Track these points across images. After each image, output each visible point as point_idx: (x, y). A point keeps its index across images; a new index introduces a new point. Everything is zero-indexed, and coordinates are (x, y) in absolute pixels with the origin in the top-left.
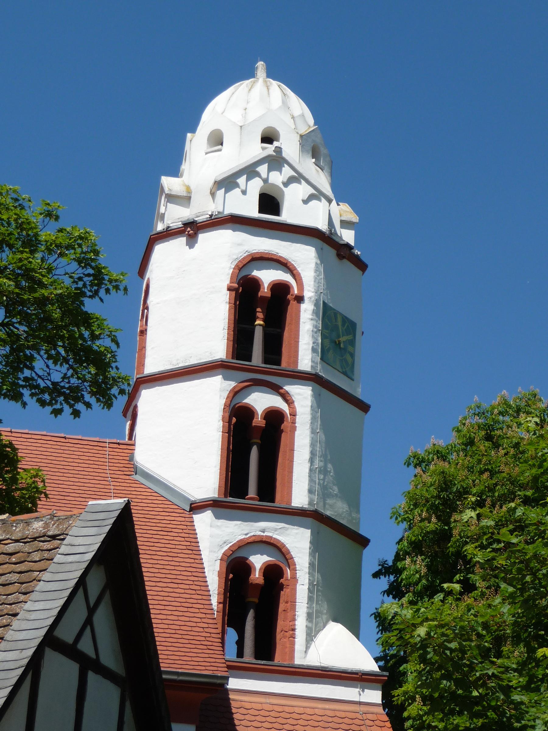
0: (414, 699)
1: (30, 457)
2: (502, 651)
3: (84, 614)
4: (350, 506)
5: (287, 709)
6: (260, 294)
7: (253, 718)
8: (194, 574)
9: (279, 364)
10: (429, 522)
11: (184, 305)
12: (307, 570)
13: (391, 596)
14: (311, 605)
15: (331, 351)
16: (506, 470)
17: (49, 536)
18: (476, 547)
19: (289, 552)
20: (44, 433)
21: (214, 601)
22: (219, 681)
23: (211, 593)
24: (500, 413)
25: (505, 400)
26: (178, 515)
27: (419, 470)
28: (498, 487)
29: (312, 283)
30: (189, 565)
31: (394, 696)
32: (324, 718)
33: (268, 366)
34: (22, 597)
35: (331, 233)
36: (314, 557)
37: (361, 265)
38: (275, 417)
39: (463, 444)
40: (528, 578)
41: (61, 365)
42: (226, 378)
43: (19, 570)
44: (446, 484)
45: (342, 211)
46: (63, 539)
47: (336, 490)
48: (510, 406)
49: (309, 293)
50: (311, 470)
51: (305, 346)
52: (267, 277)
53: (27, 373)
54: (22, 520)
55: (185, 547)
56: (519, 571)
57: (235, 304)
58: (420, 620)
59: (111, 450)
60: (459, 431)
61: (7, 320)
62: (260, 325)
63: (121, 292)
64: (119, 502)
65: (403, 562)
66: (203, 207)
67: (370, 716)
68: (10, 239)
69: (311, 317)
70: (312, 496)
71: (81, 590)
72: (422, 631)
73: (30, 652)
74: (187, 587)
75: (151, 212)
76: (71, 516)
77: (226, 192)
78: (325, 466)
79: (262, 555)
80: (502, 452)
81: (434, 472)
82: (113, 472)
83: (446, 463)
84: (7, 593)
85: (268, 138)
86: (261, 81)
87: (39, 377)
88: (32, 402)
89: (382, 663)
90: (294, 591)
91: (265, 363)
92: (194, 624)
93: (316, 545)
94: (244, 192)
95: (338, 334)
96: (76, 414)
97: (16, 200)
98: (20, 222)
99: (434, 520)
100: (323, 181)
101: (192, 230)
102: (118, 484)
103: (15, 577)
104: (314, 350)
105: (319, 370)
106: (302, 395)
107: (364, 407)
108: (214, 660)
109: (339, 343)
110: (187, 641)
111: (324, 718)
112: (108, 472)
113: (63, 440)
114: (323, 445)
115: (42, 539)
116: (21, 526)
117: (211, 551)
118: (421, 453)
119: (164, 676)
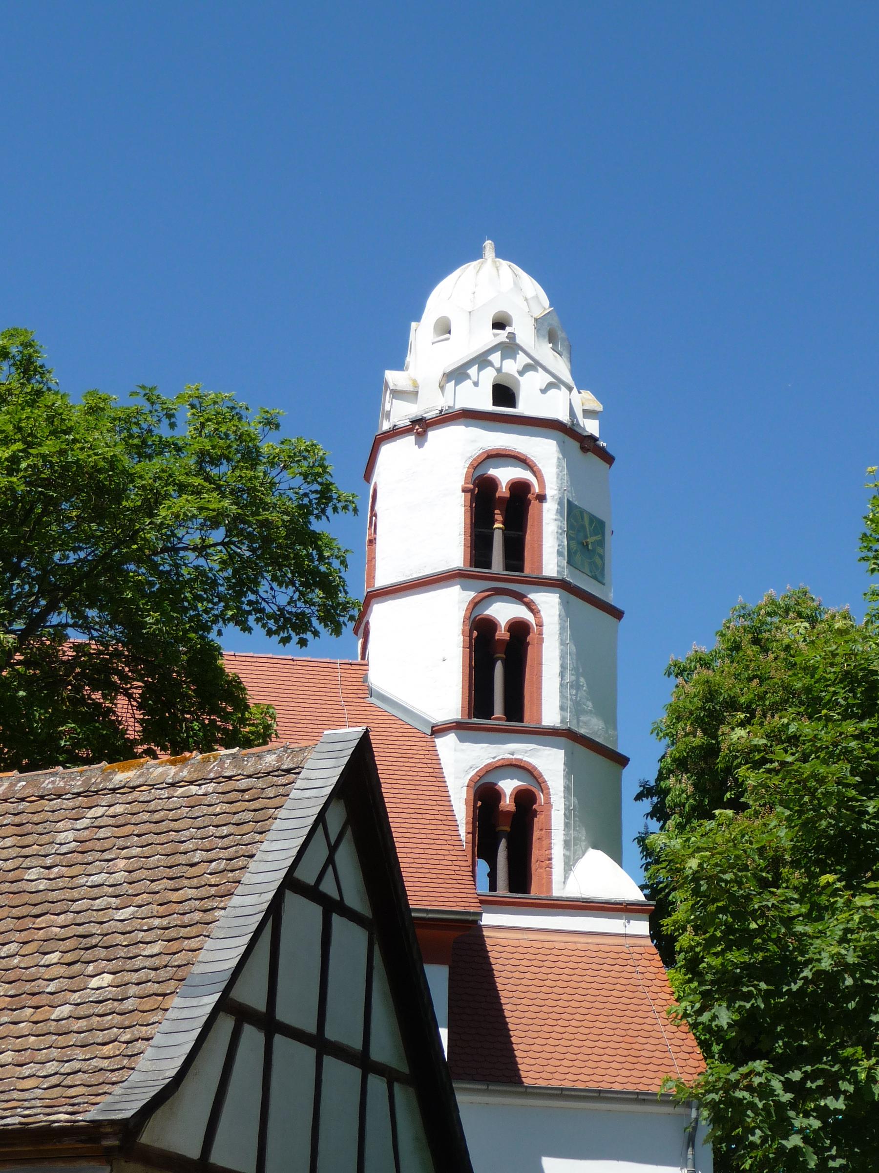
0: (684, 929)
2: (781, 873)
3: (325, 853)
4: (606, 722)
5: (546, 945)
6: (497, 495)
7: (511, 956)
8: (439, 803)
9: (522, 570)
10: (695, 737)
12: (562, 795)
13: (655, 819)
14: (568, 831)
15: (578, 554)
16: (778, 675)
17: (283, 770)
18: (748, 769)
19: (541, 775)
20: (270, 655)
21: (463, 831)
22: (471, 918)
23: (458, 822)
24: (768, 614)
25: (773, 600)
26: (418, 739)
27: (680, 680)
28: (769, 695)
29: (555, 479)
30: (433, 793)
31: (663, 926)
32: (587, 953)
33: (509, 573)
34: (258, 837)
35: (573, 424)
36: (569, 780)
37: (607, 458)
38: (519, 629)
39: (728, 649)
40: (806, 799)
41: (287, 587)
42: (464, 588)
43: (253, 808)
44: (711, 695)
45: (585, 400)
46: (299, 773)
47: (590, 705)
49: (552, 491)
50: (561, 685)
51: (550, 550)
52: (505, 475)
53: (252, 597)
54: (254, 754)
55: (428, 774)
56: (796, 791)
57: (471, 506)
58: (691, 850)
59: (343, 671)
60: (723, 635)
61: (227, 540)
62: (498, 528)
63: (351, 513)
64: (357, 731)
65: (667, 782)
66: (431, 403)
67: (637, 949)
68: (230, 452)
69: (555, 517)
70: (564, 713)
71: (321, 827)
72: (693, 863)
73: (270, 896)
74: (433, 817)
75: (376, 410)
76: (306, 748)
77: (456, 385)
78: (577, 681)
79: (512, 779)
80: (772, 656)
81: (697, 681)
82: (346, 695)
83: (711, 671)
84: (242, 833)
86: (489, 261)
87: (264, 599)
88: (257, 628)
89: (647, 891)
90: (549, 817)
91: (506, 570)
92: (442, 857)
93: (571, 767)
94: (476, 384)
95: (586, 535)
96: (303, 643)
97: (233, 408)
98: (239, 433)
99: (699, 733)
100: (562, 367)
101: (420, 427)
102: (352, 708)
103: (249, 816)
104: (559, 553)
105: (567, 576)
106: (549, 604)
107: (617, 614)
108: (465, 895)
109: (587, 545)
110: (435, 876)
111: (587, 953)
112: (340, 695)
113: (291, 662)
114: (574, 657)
115: (276, 773)
116: (252, 760)
117: (456, 778)
118: (682, 661)
119: (413, 915)
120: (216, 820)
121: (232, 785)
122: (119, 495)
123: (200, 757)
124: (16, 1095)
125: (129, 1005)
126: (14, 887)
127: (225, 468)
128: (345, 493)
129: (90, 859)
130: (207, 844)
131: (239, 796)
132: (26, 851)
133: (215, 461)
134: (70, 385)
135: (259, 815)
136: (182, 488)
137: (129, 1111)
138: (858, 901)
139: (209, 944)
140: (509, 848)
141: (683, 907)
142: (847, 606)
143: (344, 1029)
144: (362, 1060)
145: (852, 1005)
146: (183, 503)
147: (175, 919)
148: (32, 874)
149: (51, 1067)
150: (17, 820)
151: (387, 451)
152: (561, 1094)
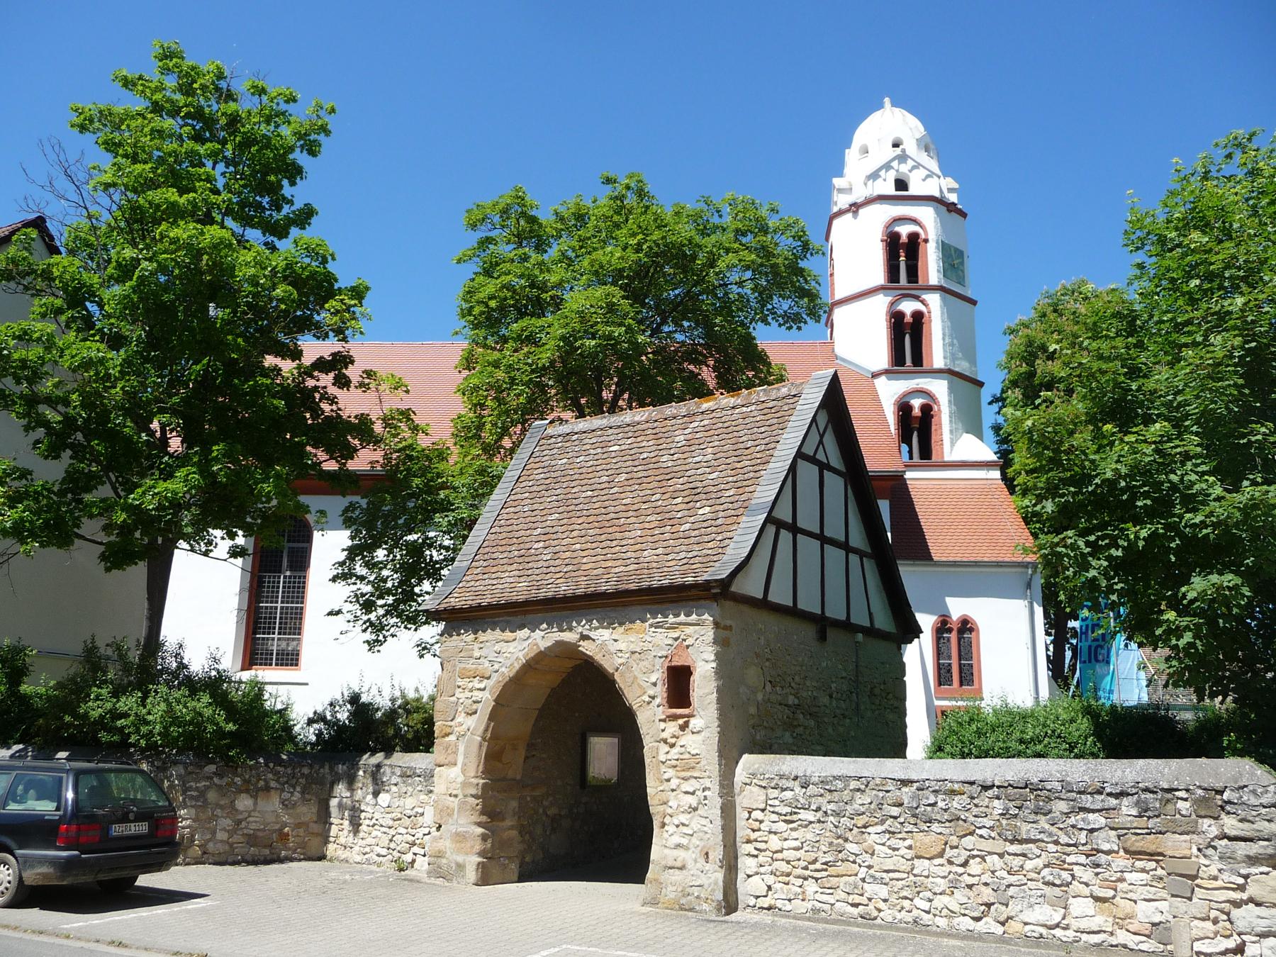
1: (775, 357)
11: (854, 256)
37: (963, 214)
38: (918, 316)
44: (1030, 343)
45: (949, 182)
49: (932, 236)
51: (932, 267)
52: (904, 230)
53: (770, 307)
64: (832, 371)
66: (859, 194)
75: (828, 201)
85: (896, 145)
88: (774, 323)
95: (953, 259)
96: (799, 328)
100: (933, 165)
101: (855, 208)
103: (775, 421)
106: (934, 300)
107: (974, 303)
118: (1013, 326)
121: (765, 405)
122: (694, 257)
125: (719, 522)
127: (750, 237)
128: (817, 246)
133: (744, 234)
134: (665, 205)
135: (780, 420)
136: (728, 251)
137: (724, 575)
138: (1126, 439)
140: (919, 436)
141: (1021, 458)
143: (834, 530)
144: (845, 546)
145: (1125, 497)
146: (731, 258)
149: (683, 555)
151: (836, 222)
152: (955, 564)
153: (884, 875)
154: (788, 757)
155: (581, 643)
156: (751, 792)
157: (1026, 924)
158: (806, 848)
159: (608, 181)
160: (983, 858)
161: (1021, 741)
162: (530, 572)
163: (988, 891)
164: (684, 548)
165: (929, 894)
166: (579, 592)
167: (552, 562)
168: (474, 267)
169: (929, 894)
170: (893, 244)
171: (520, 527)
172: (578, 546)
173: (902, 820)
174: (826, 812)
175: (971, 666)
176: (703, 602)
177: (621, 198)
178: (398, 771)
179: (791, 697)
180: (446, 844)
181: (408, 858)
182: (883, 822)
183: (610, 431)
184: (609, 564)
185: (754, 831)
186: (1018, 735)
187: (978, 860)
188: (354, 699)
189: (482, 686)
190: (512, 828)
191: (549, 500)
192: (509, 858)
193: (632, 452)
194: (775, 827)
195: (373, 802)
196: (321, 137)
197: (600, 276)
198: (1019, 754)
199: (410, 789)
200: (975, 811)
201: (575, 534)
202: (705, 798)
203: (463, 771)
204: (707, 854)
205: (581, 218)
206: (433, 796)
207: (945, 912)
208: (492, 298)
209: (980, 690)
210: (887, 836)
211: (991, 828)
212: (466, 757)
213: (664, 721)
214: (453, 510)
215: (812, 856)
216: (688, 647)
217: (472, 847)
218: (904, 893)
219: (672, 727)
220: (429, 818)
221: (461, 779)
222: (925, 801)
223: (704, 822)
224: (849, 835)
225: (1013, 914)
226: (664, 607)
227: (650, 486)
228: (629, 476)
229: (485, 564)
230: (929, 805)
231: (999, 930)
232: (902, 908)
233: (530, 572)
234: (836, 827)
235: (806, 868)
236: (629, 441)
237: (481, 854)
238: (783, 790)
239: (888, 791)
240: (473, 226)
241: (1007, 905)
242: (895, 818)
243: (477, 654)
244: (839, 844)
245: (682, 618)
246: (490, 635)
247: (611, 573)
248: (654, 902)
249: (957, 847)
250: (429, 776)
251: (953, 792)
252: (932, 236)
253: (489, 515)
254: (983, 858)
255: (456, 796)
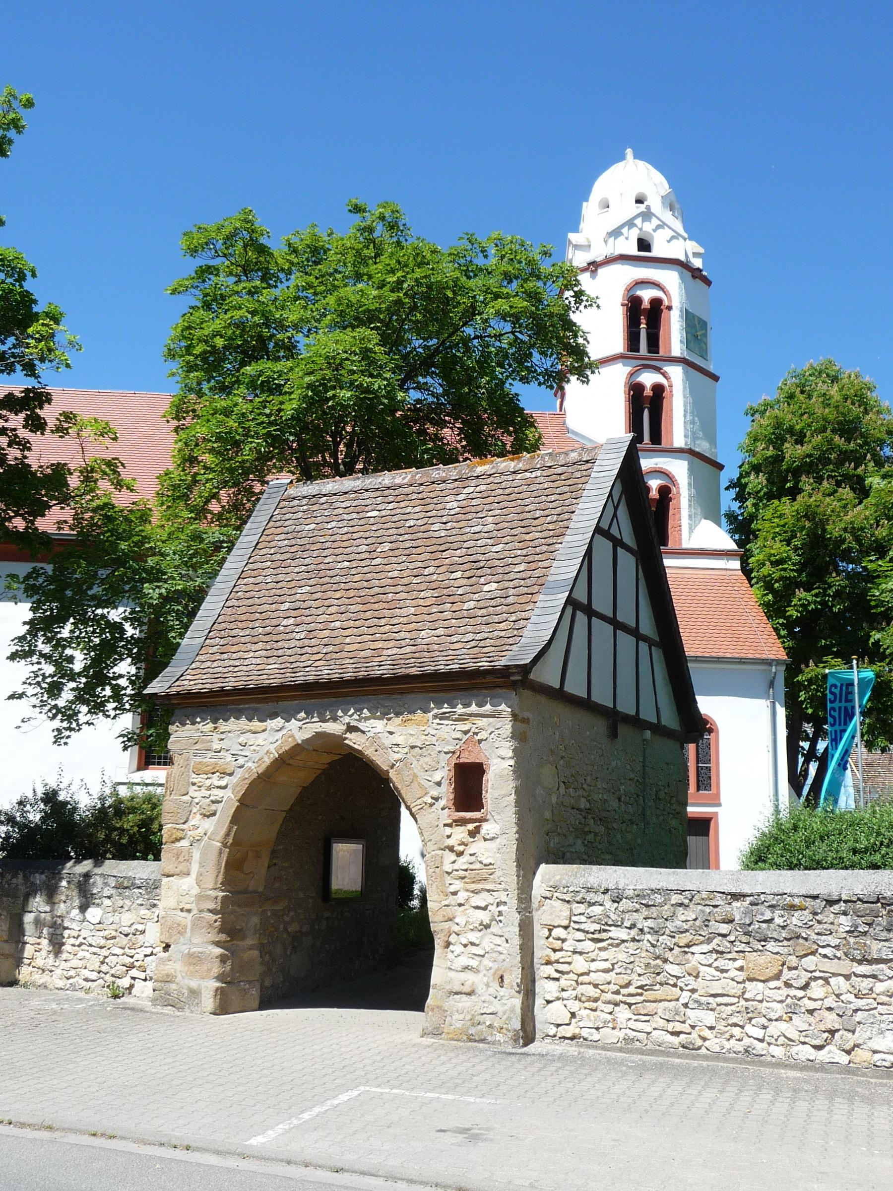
24: (810, 375)
34: (575, 501)
37: (708, 282)
38: (658, 389)
44: (778, 425)
45: (692, 247)
48: (816, 370)
49: (676, 303)
51: (675, 339)
52: (647, 295)
66: (598, 252)
78: (693, 419)
85: (639, 201)
93: (691, 470)
94: (627, 238)
99: (771, 448)
100: (678, 226)
104: (681, 342)
106: (676, 372)
107: (716, 378)
116: (562, 456)
120: (546, 492)
121: (552, 471)
123: (528, 455)
124: (451, 652)
125: (511, 600)
126: (426, 535)
129: (470, 517)
130: (542, 506)
131: (558, 477)
132: (429, 514)
135: (573, 488)
136: (497, 296)
139: (555, 564)
142: (858, 369)
143: (626, 616)
144: (634, 632)
147: (530, 550)
148: (436, 527)
149: (470, 637)
150: (420, 496)
153: (711, 1000)
154: (595, 868)
155: (348, 735)
156: (552, 907)
157: (875, 1052)
158: (618, 970)
159: (357, 209)
160: (826, 981)
161: (855, 851)
162: (280, 652)
163: (832, 1016)
164: (470, 629)
165: (763, 1021)
166: (348, 676)
167: (307, 642)
168: (193, 299)
169: (763, 1021)
170: (633, 307)
171: (263, 600)
172: (338, 624)
173: (732, 938)
174: (641, 930)
175: (709, 769)
176: (499, 691)
177: (370, 230)
178: (112, 882)
179: (583, 800)
180: (176, 966)
181: (125, 982)
182: (709, 941)
183: (366, 495)
184: (379, 645)
185: (555, 950)
186: (850, 843)
187: (821, 982)
188: (50, 797)
189: (223, 783)
190: (251, 948)
191: (296, 569)
192: (250, 982)
193: (395, 518)
194: (580, 947)
195: (79, 917)
196: (12, 134)
197: (353, 318)
198: (852, 866)
199: (128, 902)
200: (818, 928)
201: (333, 609)
202: (500, 913)
203: (198, 882)
204: (502, 977)
205: (317, 253)
206: (157, 911)
207: (782, 1040)
208: (217, 334)
209: (717, 795)
210: (715, 956)
211: (837, 947)
212: (202, 864)
213: (450, 825)
214: (165, 581)
215: (625, 979)
216: (480, 741)
217: (209, 970)
218: (734, 1020)
219: (460, 834)
220: (153, 935)
221: (196, 890)
222: (759, 918)
223: (498, 940)
224: (669, 956)
225: (860, 1041)
226: (451, 695)
227: (421, 558)
228: (394, 546)
229: (222, 642)
230: (765, 922)
231: (844, 1059)
232: (732, 1036)
233: (280, 652)
234: (653, 946)
235: (617, 993)
236: (391, 506)
237: (219, 978)
238: (591, 904)
239: (716, 906)
240: (194, 252)
241: (853, 1032)
242: (724, 936)
243: (216, 746)
244: (657, 966)
245: (474, 708)
246: (232, 724)
247: (385, 657)
248: (436, 1032)
249: (796, 968)
250: (152, 887)
251: (792, 908)
252: (676, 303)
253: (222, 586)
254: (826, 981)
255: (189, 911)
